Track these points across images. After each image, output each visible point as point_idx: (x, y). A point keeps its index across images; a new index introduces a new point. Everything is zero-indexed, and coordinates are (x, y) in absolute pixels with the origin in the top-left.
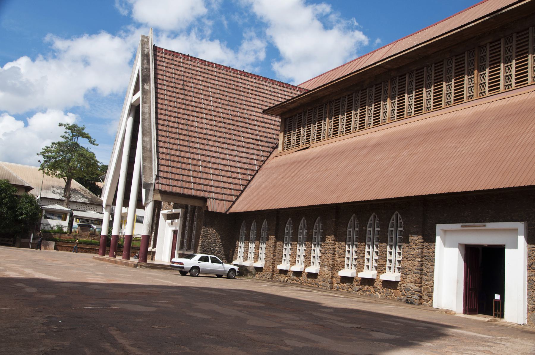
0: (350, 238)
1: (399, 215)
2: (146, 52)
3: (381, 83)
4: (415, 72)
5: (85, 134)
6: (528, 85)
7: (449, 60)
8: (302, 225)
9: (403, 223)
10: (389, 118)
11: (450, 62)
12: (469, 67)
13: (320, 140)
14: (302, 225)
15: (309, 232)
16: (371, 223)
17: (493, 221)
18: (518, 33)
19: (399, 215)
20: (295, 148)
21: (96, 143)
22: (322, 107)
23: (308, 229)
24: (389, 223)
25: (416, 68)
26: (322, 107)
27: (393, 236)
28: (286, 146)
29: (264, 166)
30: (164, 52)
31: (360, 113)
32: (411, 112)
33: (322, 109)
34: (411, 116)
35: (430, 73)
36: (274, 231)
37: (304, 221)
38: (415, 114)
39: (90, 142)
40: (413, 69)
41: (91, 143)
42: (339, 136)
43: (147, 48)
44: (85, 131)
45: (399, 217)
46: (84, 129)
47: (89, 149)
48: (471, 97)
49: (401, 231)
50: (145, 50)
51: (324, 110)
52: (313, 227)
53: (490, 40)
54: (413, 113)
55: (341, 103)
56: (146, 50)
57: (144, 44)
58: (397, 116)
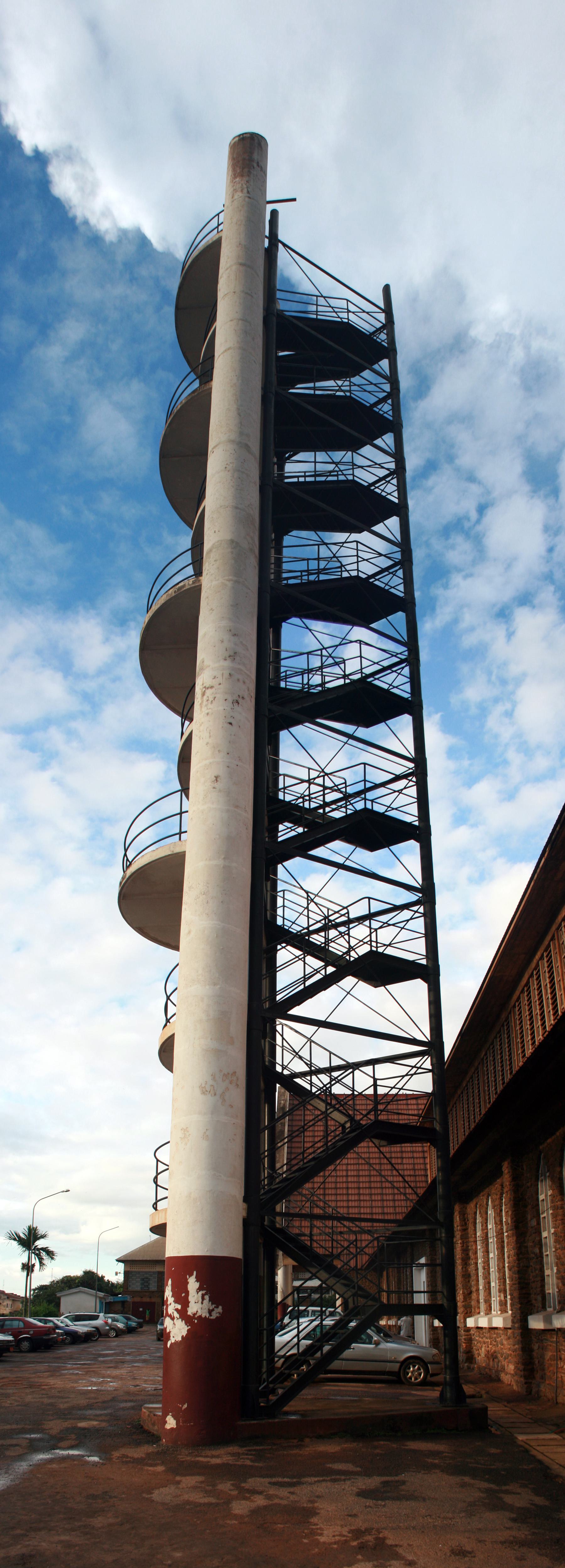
2: (282, 1105)
50: (281, 1103)
56: (282, 1102)
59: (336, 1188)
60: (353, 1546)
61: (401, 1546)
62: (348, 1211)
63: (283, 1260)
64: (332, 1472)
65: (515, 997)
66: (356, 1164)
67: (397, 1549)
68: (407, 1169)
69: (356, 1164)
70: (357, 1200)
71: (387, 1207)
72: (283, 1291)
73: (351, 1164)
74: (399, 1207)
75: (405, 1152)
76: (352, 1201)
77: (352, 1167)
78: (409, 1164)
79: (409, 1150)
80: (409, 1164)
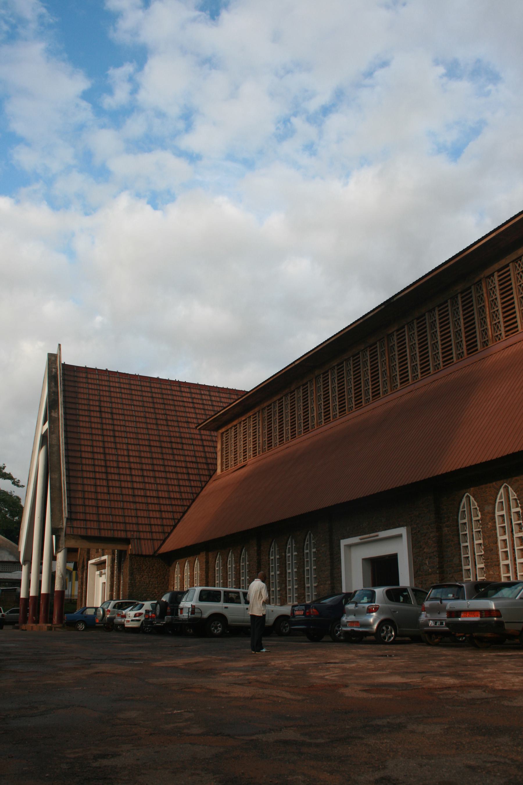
0: (308, 561)
1: (472, 498)
2: (53, 374)
3: (376, 343)
4: (336, 368)
5: (5, 473)
6: (430, 374)
7: (478, 285)
8: (308, 543)
9: (478, 508)
10: (317, 423)
11: (412, 328)
12: (517, 283)
13: (295, 437)
14: (308, 543)
15: (237, 566)
16: (502, 502)
17: (386, 530)
18: (417, 319)
19: (472, 498)
20: (252, 458)
21: (21, 484)
22: (446, 305)
23: (236, 562)
24: (496, 503)
25: (336, 364)
26: (446, 305)
27: (506, 524)
28: (224, 467)
29: (202, 494)
30: (75, 370)
31: (291, 419)
32: (439, 364)
33: (424, 322)
34: (440, 369)
35: (481, 293)
36: (204, 570)
37: (275, 544)
38: (444, 366)
39: (14, 483)
40: (334, 365)
41: (15, 485)
42: (230, 469)
43: (54, 368)
44: (6, 471)
45: (472, 501)
46: (4, 468)
47: (13, 493)
48: (386, 391)
49: (518, 513)
50: (52, 371)
51: (345, 370)
52: (240, 559)
53: (395, 329)
54: (441, 364)
55: (272, 409)
56: (54, 370)
57: (52, 363)
58: (444, 362)
59: (118, 467)
60: (403, 600)
61: (346, 686)
62: (134, 492)
63: (65, 541)
64: (241, 671)
65: (487, 272)
66: (137, 445)
67: (342, 690)
68: (188, 456)
69: (137, 445)
70: (142, 483)
71: (173, 492)
72: (63, 577)
73: (131, 444)
74: (184, 492)
75: (184, 438)
76: (136, 482)
77: (133, 447)
78: (190, 450)
79: (188, 436)
80: (190, 450)
